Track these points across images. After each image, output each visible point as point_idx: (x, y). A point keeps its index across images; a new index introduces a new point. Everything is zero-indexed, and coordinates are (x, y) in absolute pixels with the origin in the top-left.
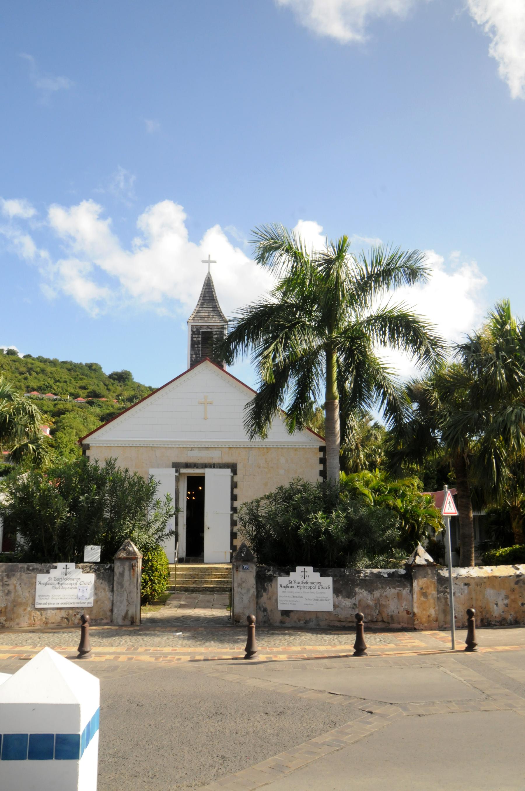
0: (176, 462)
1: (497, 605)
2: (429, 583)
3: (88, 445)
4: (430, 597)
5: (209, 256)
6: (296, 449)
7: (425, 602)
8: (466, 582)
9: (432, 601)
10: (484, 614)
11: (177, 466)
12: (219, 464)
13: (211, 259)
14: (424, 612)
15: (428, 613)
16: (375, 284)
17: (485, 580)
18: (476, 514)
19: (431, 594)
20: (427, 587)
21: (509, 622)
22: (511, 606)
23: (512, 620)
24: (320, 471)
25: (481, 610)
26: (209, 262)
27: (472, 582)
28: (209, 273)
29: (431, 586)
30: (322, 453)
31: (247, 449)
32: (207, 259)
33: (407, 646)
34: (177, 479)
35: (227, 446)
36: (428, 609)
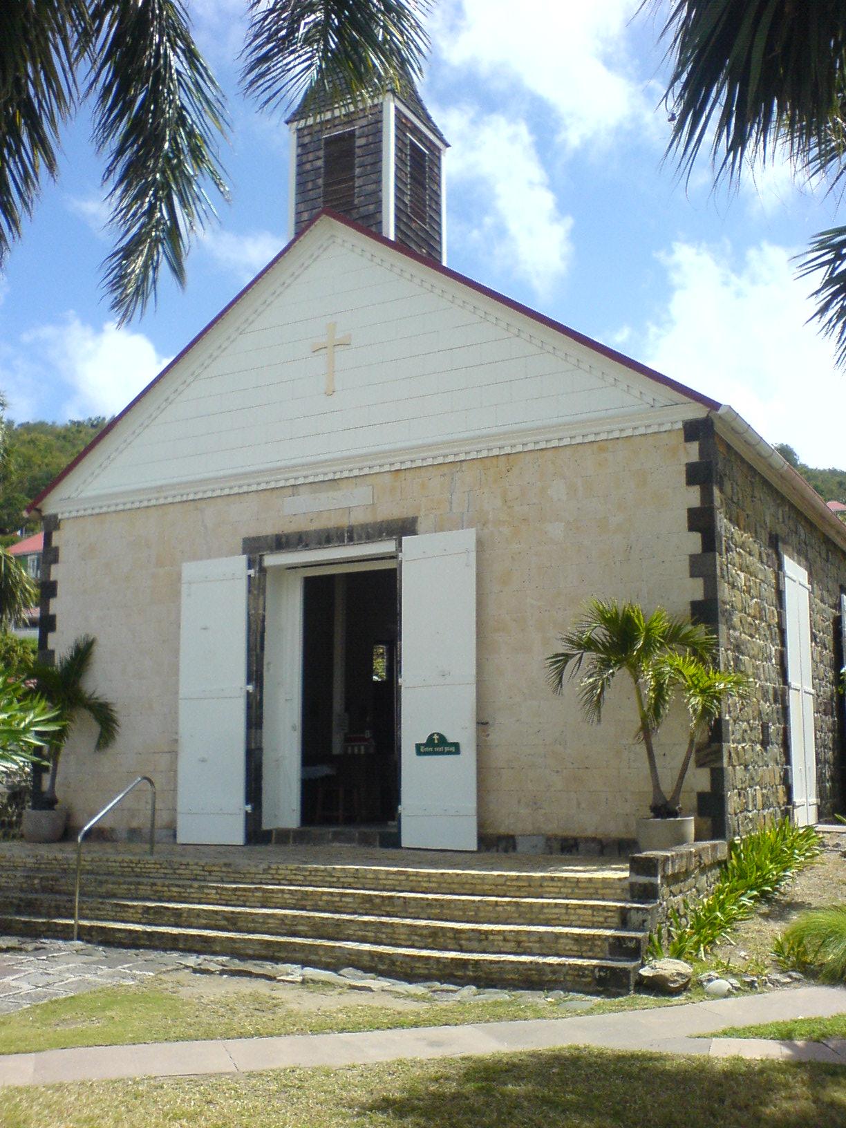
0: (253, 534)
3: (55, 516)
6: (601, 446)
11: (255, 548)
12: (364, 527)
16: (819, 156)
18: (652, 880)
24: (692, 512)
30: (694, 447)
31: (445, 470)
34: (257, 587)
35: (387, 468)
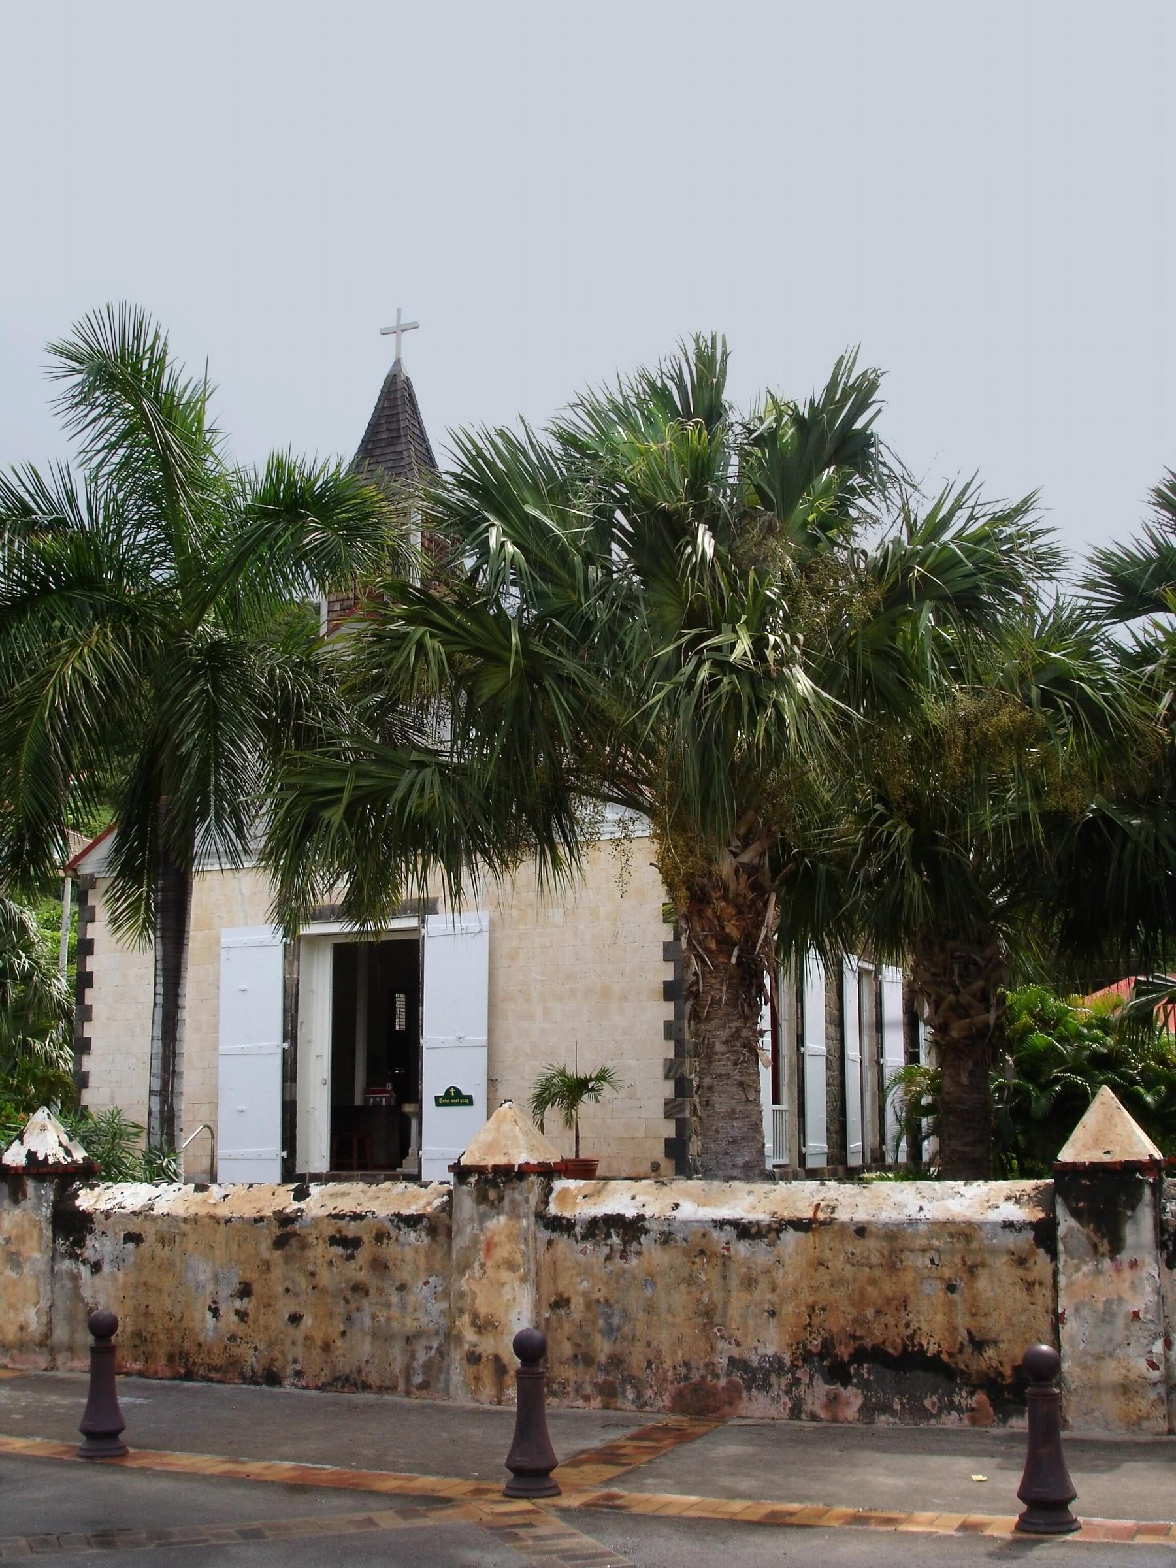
1: (215, 1312)
2: (27, 1225)
4: (27, 1269)
5: (399, 311)
7: (14, 1284)
8: (133, 1228)
9: (30, 1282)
10: (177, 1335)
13: (404, 321)
14: (12, 1314)
15: (21, 1318)
17: (185, 1227)
19: (28, 1258)
20: (21, 1239)
21: (249, 1374)
22: (256, 1321)
23: (257, 1367)
25: (171, 1324)
26: (399, 330)
27: (149, 1232)
28: (398, 363)
29: (31, 1237)
32: (391, 323)
33: (1047, 1524)
34: (291, 955)
36: (20, 1306)
